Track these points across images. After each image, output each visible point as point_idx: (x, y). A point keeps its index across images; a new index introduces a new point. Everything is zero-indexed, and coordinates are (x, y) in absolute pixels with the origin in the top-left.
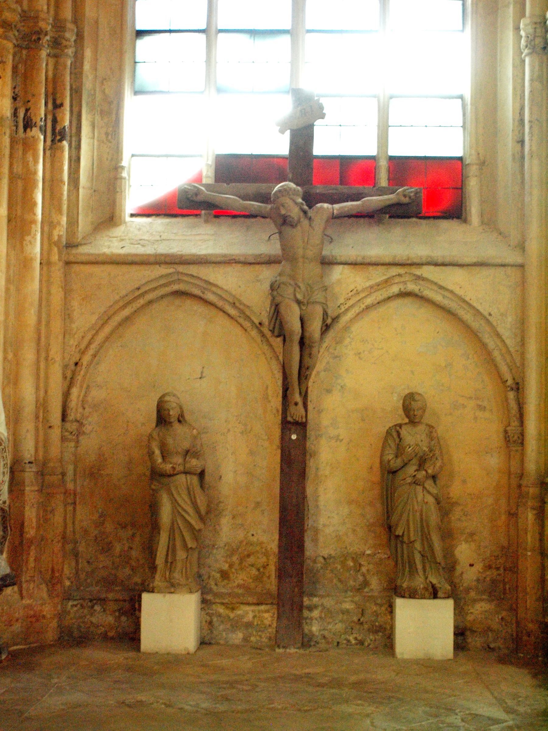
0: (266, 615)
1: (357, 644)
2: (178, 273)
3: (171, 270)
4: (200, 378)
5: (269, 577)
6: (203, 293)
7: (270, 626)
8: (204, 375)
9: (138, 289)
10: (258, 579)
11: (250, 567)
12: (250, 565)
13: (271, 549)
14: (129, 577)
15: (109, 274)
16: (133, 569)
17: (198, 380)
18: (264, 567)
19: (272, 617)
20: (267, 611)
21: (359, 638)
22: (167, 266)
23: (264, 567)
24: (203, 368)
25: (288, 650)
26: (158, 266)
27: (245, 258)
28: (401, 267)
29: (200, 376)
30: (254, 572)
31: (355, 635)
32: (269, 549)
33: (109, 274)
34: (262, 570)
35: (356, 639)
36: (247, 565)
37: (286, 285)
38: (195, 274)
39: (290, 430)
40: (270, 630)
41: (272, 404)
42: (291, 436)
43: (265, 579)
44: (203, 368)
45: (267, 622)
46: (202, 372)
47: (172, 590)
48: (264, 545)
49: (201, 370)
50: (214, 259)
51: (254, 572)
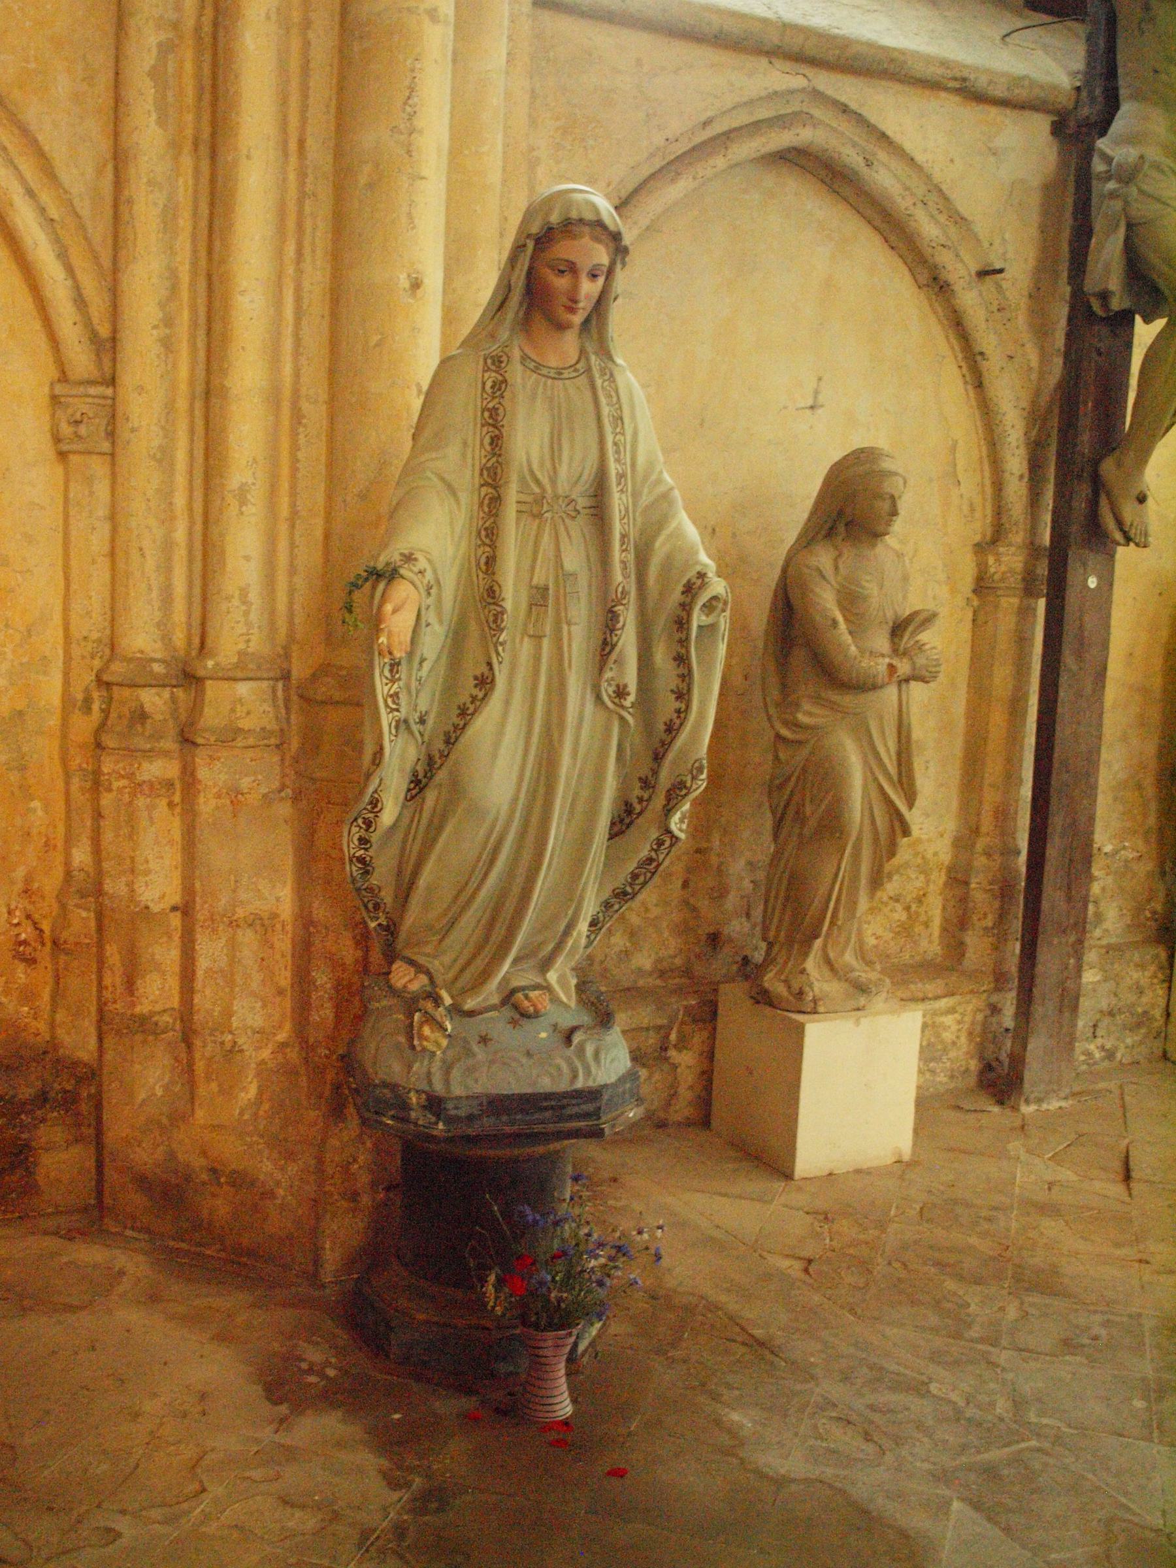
0: (949, 1020)
1: (1103, 1059)
2: (817, 95)
3: (798, 82)
4: (812, 407)
5: (926, 925)
6: (869, 165)
7: (954, 1043)
8: (821, 399)
9: (706, 124)
10: (905, 931)
11: (892, 903)
12: (891, 898)
13: (936, 854)
14: (626, 954)
15: (639, 63)
16: (632, 934)
17: (808, 412)
18: (920, 900)
19: (959, 1022)
20: (951, 1011)
21: (1108, 1046)
22: (788, 66)
23: (920, 900)
24: (820, 379)
25: (1045, 1106)
26: (764, 61)
27: (990, 82)
28: (1050, 190)
29: (810, 402)
30: (900, 915)
31: (1099, 1041)
32: (929, 856)
33: (639, 63)
34: (914, 907)
35: (1103, 1048)
36: (885, 899)
37: (1163, 172)
38: (853, 106)
39: (1084, 564)
40: (952, 1054)
41: (963, 489)
42: (1086, 580)
43: (918, 929)
44: (820, 379)
45: (948, 1036)
46: (816, 393)
47: (862, 1001)
48: (921, 848)
49: (815, 386)
50: (920, 69)
51: (900, 915)
